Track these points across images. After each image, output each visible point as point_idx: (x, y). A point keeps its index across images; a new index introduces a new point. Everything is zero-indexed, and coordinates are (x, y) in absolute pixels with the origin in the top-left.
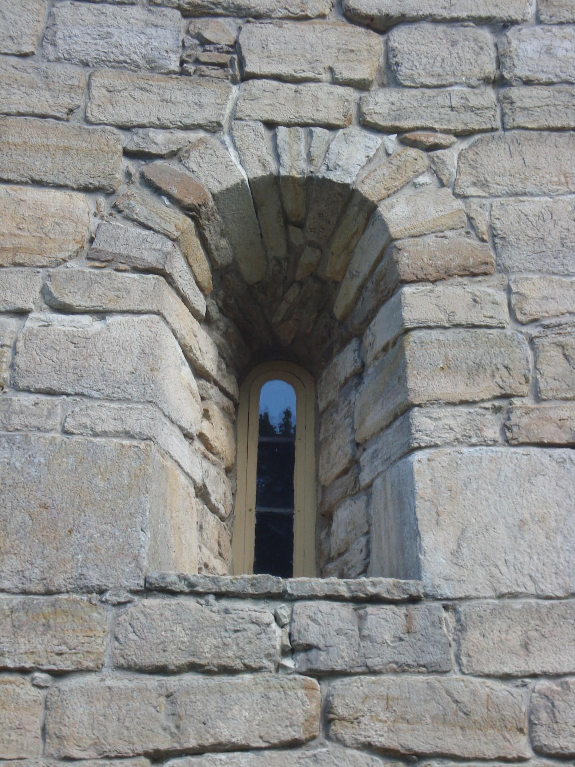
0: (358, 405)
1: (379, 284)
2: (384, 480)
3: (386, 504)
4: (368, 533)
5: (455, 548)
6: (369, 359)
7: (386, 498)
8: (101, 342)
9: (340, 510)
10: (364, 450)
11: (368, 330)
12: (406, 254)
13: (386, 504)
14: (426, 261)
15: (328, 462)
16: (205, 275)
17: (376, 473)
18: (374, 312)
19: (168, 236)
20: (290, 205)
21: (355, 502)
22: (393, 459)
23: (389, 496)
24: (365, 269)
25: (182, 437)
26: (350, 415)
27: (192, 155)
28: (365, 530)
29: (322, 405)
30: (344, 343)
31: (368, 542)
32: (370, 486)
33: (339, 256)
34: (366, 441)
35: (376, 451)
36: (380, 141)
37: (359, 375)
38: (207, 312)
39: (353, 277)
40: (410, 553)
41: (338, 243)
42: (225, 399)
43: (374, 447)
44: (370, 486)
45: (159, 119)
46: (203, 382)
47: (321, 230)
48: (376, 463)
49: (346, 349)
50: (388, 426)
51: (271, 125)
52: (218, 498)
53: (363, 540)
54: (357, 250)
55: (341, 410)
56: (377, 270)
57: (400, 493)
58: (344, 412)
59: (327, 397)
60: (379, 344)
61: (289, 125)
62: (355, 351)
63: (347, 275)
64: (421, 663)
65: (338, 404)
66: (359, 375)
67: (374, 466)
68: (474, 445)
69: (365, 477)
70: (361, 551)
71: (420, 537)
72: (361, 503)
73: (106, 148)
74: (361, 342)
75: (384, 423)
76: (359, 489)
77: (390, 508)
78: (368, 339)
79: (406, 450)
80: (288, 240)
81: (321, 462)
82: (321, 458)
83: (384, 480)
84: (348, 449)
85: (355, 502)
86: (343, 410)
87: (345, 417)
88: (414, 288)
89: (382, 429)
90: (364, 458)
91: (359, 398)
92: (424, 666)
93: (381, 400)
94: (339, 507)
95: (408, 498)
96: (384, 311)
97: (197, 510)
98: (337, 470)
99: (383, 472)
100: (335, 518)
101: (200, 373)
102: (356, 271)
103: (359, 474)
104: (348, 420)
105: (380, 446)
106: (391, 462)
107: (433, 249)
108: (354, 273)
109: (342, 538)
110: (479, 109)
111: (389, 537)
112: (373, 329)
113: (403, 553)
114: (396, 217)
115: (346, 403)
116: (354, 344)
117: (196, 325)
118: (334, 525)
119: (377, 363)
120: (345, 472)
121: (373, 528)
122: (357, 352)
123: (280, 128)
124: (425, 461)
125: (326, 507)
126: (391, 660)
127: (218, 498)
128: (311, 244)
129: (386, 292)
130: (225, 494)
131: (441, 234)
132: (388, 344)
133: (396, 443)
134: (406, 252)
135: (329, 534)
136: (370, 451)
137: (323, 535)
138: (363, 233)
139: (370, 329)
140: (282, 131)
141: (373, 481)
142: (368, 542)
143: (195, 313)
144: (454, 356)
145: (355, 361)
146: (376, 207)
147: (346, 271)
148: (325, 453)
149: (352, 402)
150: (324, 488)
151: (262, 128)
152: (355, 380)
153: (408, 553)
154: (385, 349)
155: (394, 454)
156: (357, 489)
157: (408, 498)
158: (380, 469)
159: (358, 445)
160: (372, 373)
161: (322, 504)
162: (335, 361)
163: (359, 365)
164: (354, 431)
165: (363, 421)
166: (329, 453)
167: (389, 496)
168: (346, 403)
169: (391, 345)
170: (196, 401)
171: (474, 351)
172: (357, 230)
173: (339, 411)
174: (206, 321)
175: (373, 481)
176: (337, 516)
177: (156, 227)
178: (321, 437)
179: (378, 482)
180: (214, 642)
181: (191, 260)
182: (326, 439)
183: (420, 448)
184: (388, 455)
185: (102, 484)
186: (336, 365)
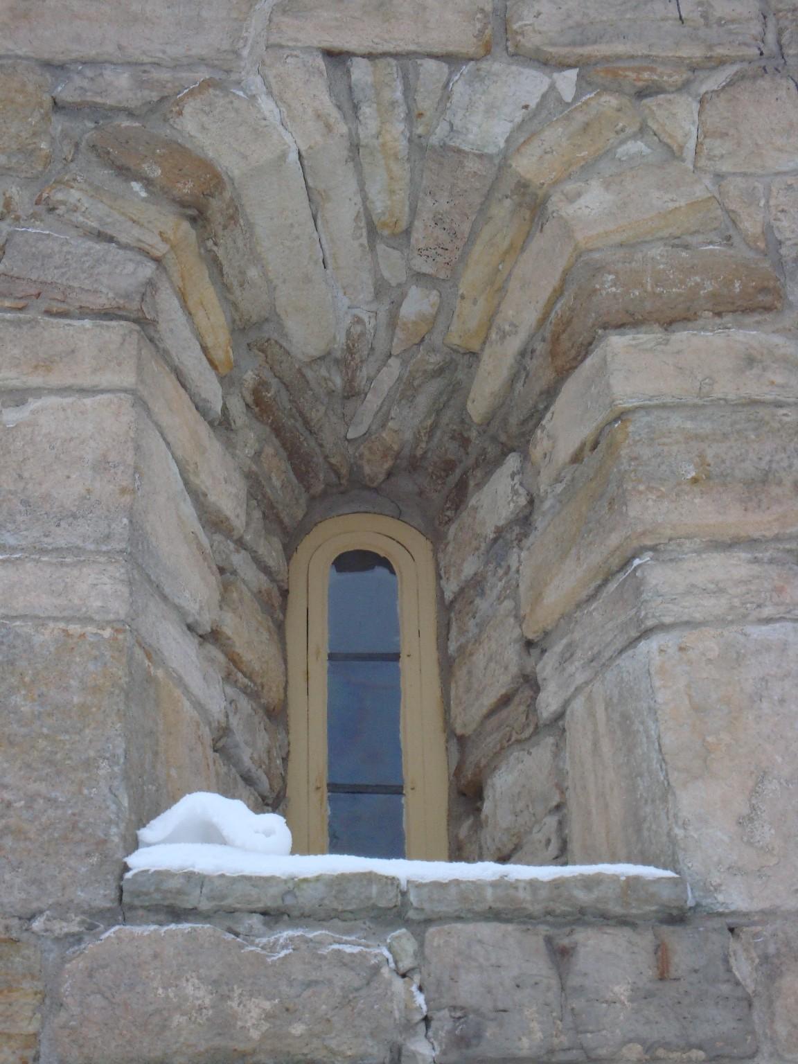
0: (526, 571)
1: (558, 339)
2: (589, 698)
3: (596, 744)
4: (558, 807)
5: (745, 810)
6: (543, 486)
7: (595, 732)
8: (19, 444)
9: (497, 773)
10: (544, 651)
11: (539, 432)
12: (611, 277)
13: (596, 744)
14: (649, 288)
15: (468, 690)
16: (220, 339)
17: (572, 689)
18: (551, 393)
19: (147, 254)
20: (379, 203)
21: (530, 753)
22: (607, 654)
23: (602, 729)
24: (530, 317)
25: (185, 628)
26: (512, 592)
27: (187, 110)
28: (556, 800)
29: (451, 588)
30: (490, 465)
31: (561, 824)
32: (560, 715)
33: (475, 302)
34: (546, 634)
35: (569, 645)
36: (546, 81)
37: (524, 521)
38: (225, 409)
39: (504, 336)
40: (654, 827)
41: (473, 275)
42: (263, 577)
43: (564, 641)
44: (560, 715)
45: (120, 48)
46: (218, 537)
47: (440, 251)
48: (571, 669)
49: (495, 477)
50: (592, 598)
51: (336, 57)
52: (256, 756)
53: (552, 821)
54: (513, 285)
55: (491, 589)
56: (553, 315)
57: (625, 717)
58: (495, 592)
59: (459, 571)
60: (565, 449)
61: (370, 56)
62: (513, 476)
63: (493, 336)
64: (693, 1040)
65: (485, 578)
66: (524, 521)
67: (566, 675)
68: (768, 620)
69: (549, 702)
70: (548, 842)
71: (674, 794)
72: (542, 752)
73: (20, 98)
74: (526, 456)
75: (584, 594)
76: (537, 727)
77: (606, 747)
78: (537, 453)
79: (634, 634)
80: (375, 271)
81: (453, 693)
82: (453, 685)
83: (589, 698)
84: (512, 654)
85: (530, 753)
86: (495, 586)
87: (500, 599)
88: (630, 336)
89: (578, 606)
90: (546, 667)
91: (524, 561)
92: (700, 1047)
93: (573, 551)
94: (495, 768)
95: (642, 723)
96: (571, 388)
97: (217, 774)
98: (489, 700)
99: (586, 683)
100: (488, 793)
101: (214, 522)
102: (512, 324)
103: (534, 699)
104: (508, 604)
105: (577, 636)
106: (599, 663)
107: (662, 266)
108: (507, 328)
109: (504, 825)
110: (733, 21)
111: (606, 806)
112: (548, 426)
113: (639, 831)
114: (587, 211)
115: (501, 572)
116: (513, 461)
117: (204, 430)
118: (487, 807)
119: (560, 488)
120: (505, 701)
121: (570, 794)
122: (517, 478)
123: (356, 60)
124: (672, 650)
125: (469, 773)
126: (632, 1035)
127: (256, 756)
128: (419, 277)
129: (573, 352)
130: (269, 752)
131: (676, 241)
132: (581, 449)
133: (610, 626)
134: (610, 273)
135: (478, 826)
136: (558, 648)
137: (463, 831)
138: (523, 249)
139: (544, 428)
140: (360, 71)
141: (567, 703)
142: (561, 824)
143: (201, 408)
144: (716, 456)
145: (515, 492)
146: (547, 198)
147: (489, 328)
148: (461, 674)
149: (513, 569)
150: (462, 741)
151: (320, 62)
152: (517, 530)
153: (649, 829)
154: (577, 458)
155: (608, 645)
156: (531, 729)
157: (642, 723)
158: (580, 678)
159: (529, 644)
160: (553, 506)
161: (458, 772)
162: (473, 502)
163: (523, 501)
164: (520, 619)
165: (538, 598)
166: (470, 672)
167: (602, 729)
168: (501, 572)
169: (587, 448)
170: (210, 568)
171: (756, 446)
172: (511, 245)
173: (488, 592)
174: (222, 425)
175: (567, 703)
176: (493, 786)
177: (123, 238)
178: (452, 647)
179: (578, 705)
180: (267, 1005)
181: (191, 304)
182: (461, 649)
183: (662, 627)
184: (596, 650)
185: (26, 708)
186: (475, 509)
